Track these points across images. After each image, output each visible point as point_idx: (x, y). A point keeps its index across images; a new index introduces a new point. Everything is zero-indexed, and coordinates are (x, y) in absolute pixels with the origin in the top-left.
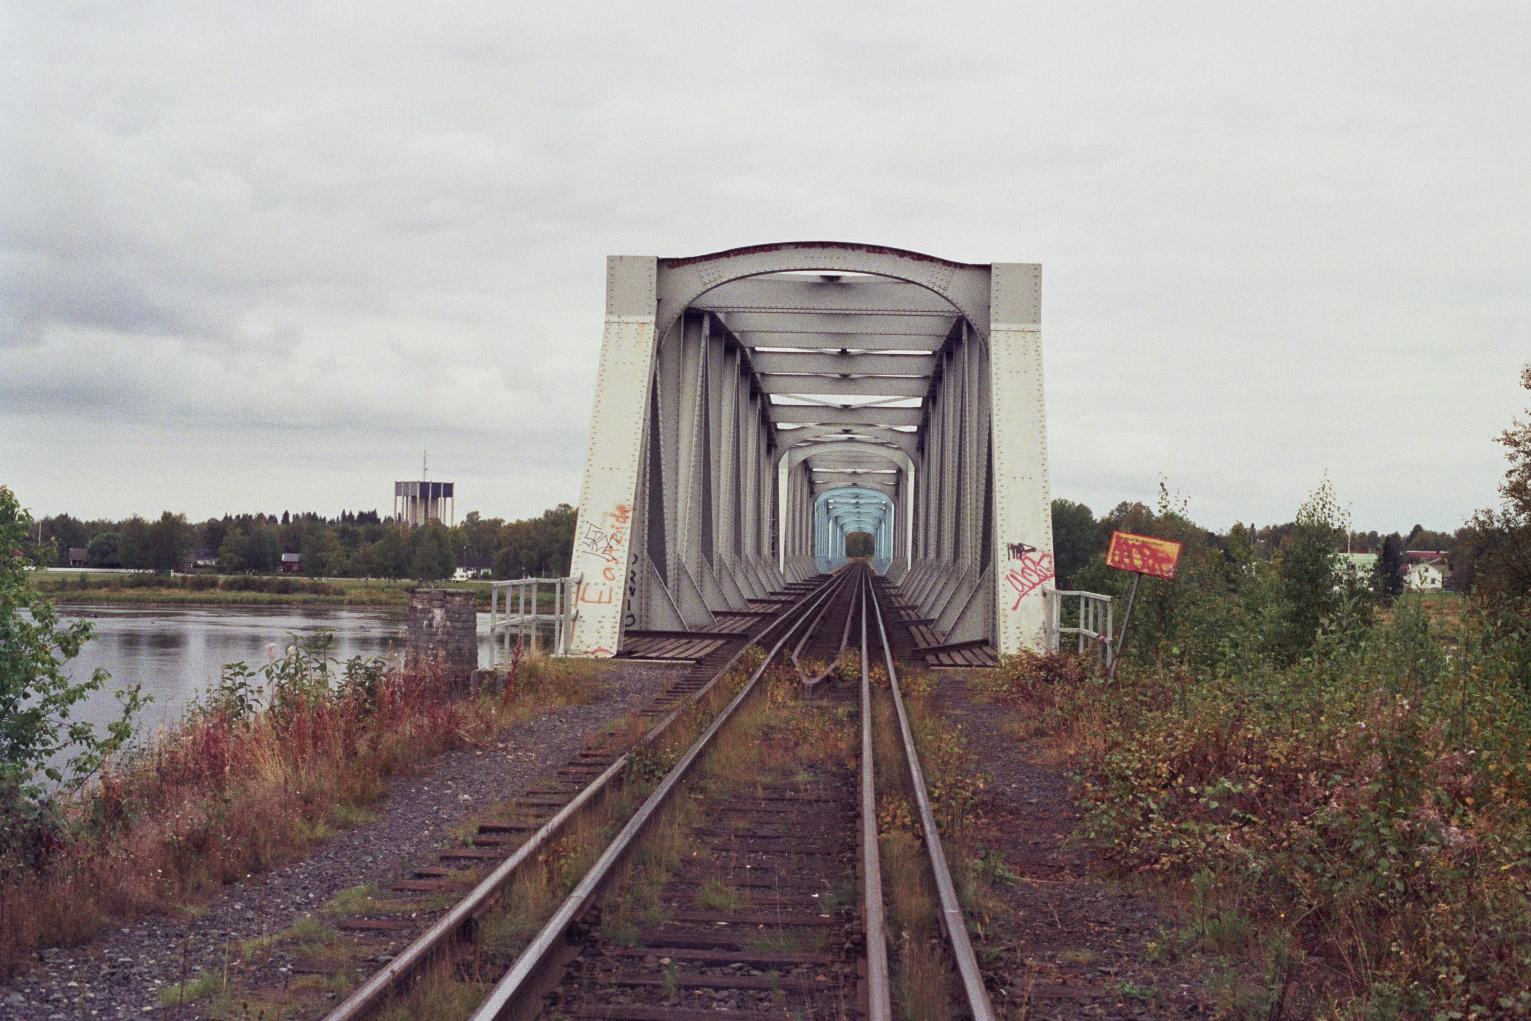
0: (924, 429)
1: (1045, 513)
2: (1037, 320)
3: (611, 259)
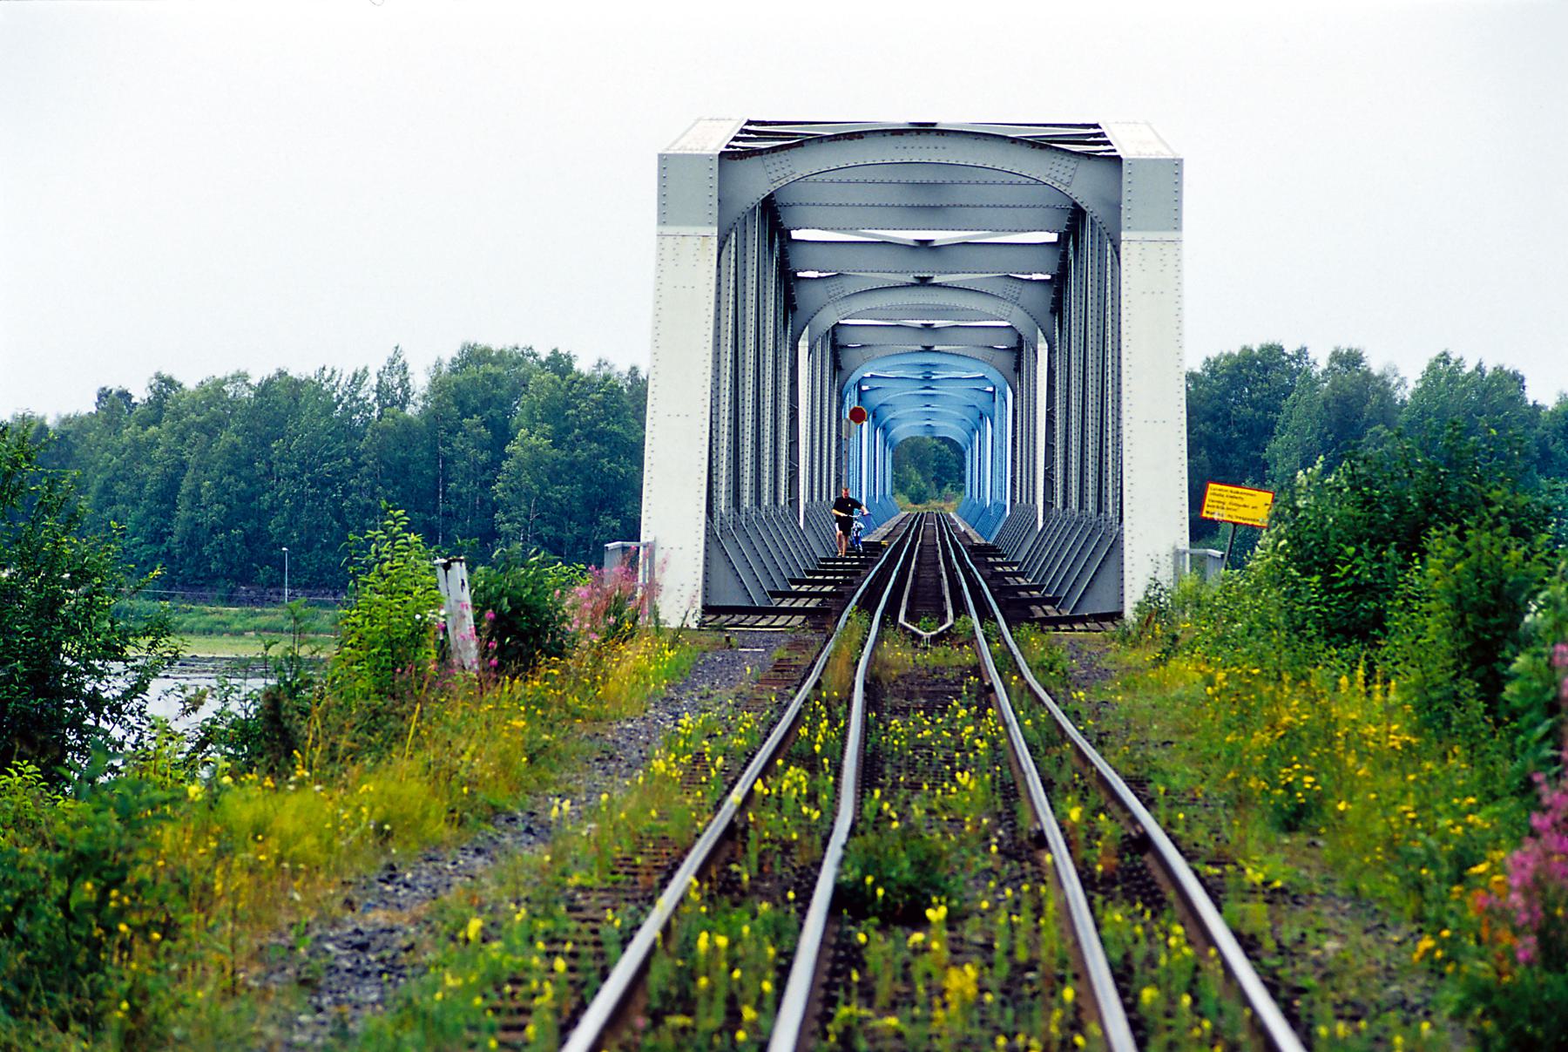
0: (1059, 283)
1: (1180, 462)
2: (1176, 224)
3: (665, 161)
